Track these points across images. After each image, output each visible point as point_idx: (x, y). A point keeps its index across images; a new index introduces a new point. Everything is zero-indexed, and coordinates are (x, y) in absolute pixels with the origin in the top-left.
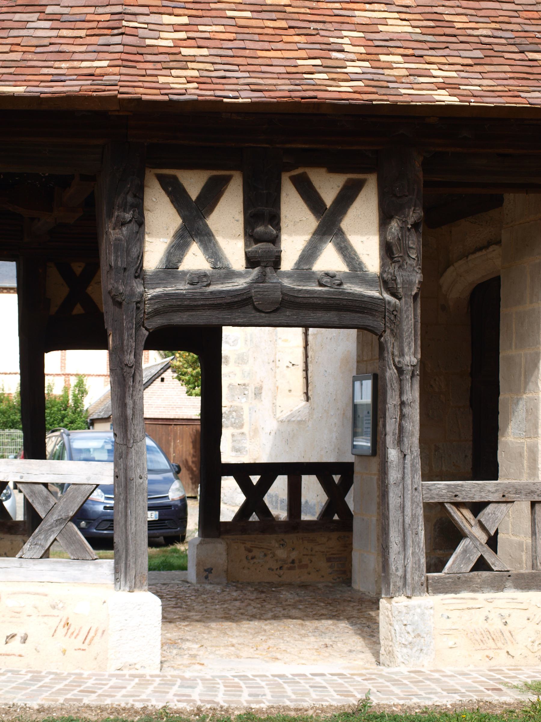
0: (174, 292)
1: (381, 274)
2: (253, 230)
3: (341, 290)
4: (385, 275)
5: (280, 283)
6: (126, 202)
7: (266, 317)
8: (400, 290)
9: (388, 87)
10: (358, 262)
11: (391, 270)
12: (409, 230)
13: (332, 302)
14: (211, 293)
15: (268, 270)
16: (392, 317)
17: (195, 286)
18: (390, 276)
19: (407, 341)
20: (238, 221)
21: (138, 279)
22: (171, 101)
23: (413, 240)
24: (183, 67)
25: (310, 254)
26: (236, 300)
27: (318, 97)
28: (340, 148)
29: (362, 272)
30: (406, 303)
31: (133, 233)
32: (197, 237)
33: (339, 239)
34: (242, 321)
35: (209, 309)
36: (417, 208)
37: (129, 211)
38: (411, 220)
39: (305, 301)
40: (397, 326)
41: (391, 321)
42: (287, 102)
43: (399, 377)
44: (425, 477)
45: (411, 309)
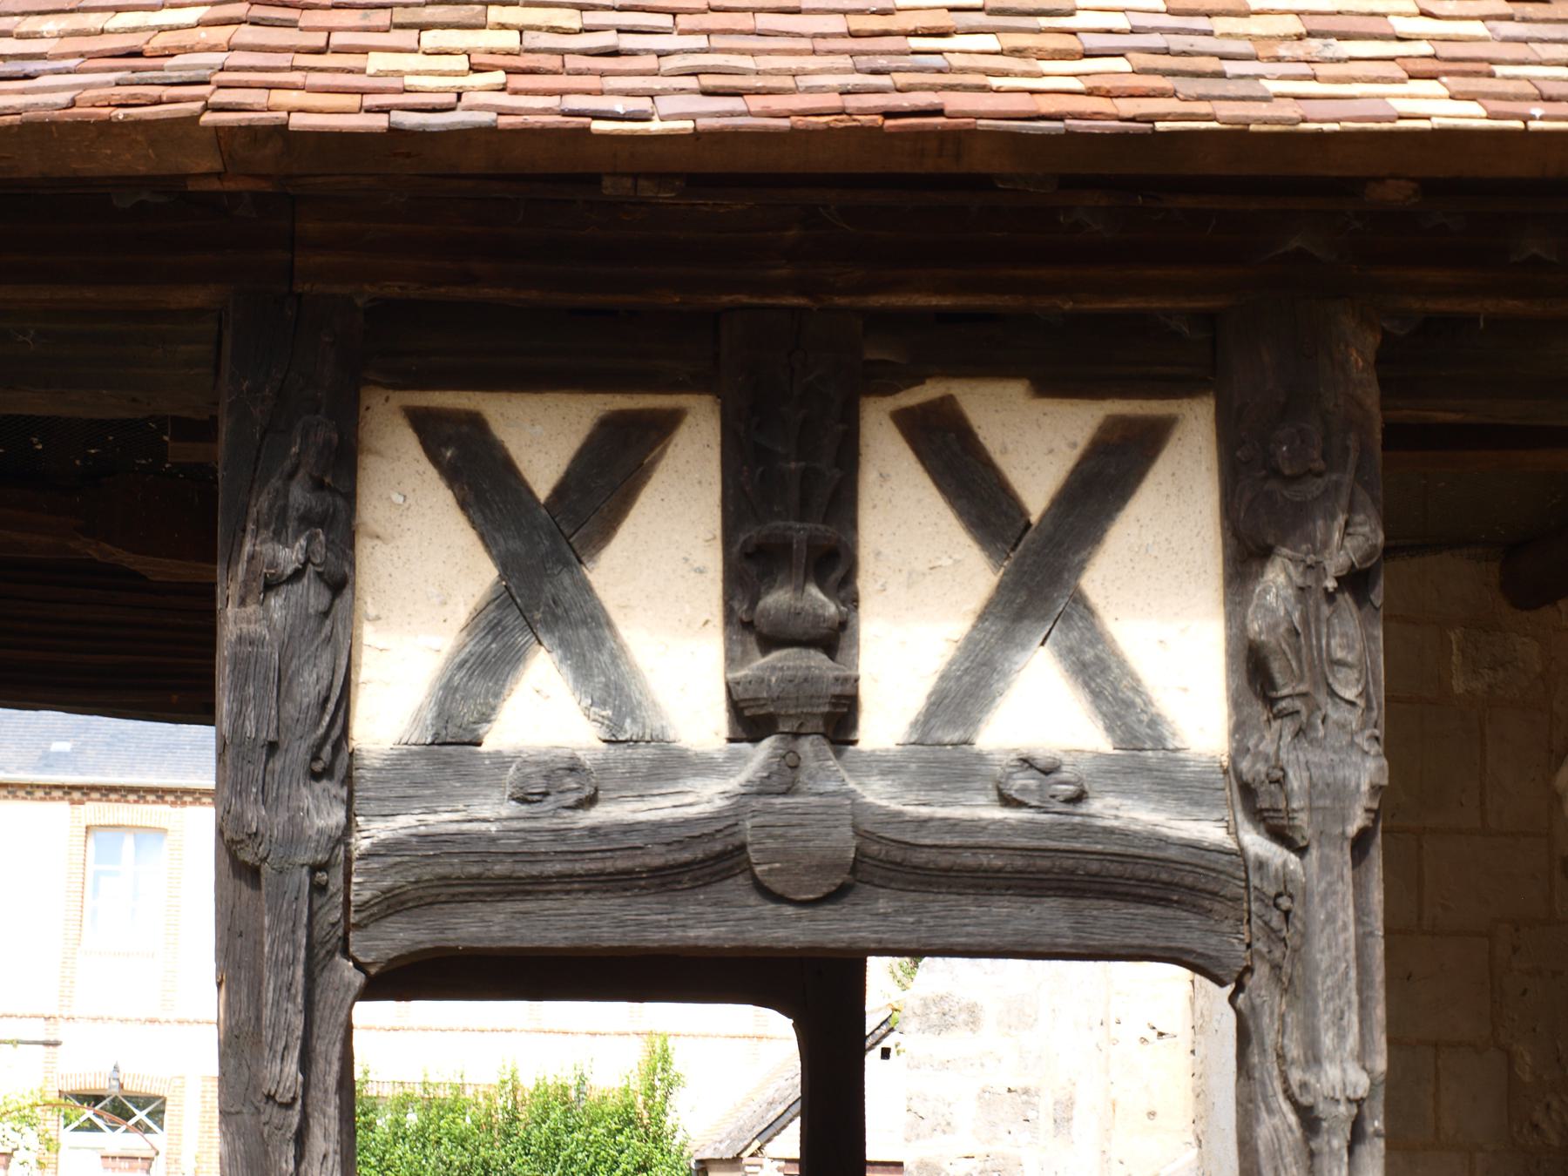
0: (454, 828)
1: (1234, 760)
2: (753, 603)
3: (1077, 819)
4: (1245, 765)
5: (849, 794)
6: (284, 509)
7: (799, 919)
8: (1302, 819)
9: (1221, 75)
10: (1145, 718)
11: (1268, 746)
12: (1330, 597)
13: (1046, 863)
14: (593, 831)
15: (806, 746)
16: (1276, 920)
17: (534, 808)
18: (1261, 767)
19: (1331, 1007)
20: (701, 571)
21: (325, 783)
22: (394, 132)
23: (1344, 635)
24: (466, 21)
25: (965, 691)
26: (686, 856)
27: (948, 108)
28: (1068, 306)
29: (1161, 754)
30: (1325, 866)
31: (308, 616)
32: (550, 630)
33: (1075, 634)
34: (710, 933)
35: (587, 891)
36: (1359, 518)
37: (296, 538)
38: (1339, 557)
39: (945, 860)
40: (1295, 951)
41: (1272, 934)
42: (829, 131)
43: (1307, 1140)
45: (1346, 890)
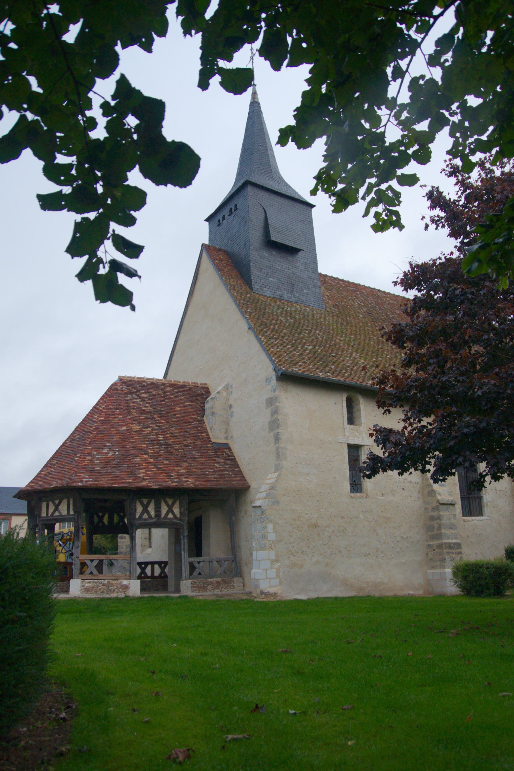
25: (167, 514)
44: (189, 557)
